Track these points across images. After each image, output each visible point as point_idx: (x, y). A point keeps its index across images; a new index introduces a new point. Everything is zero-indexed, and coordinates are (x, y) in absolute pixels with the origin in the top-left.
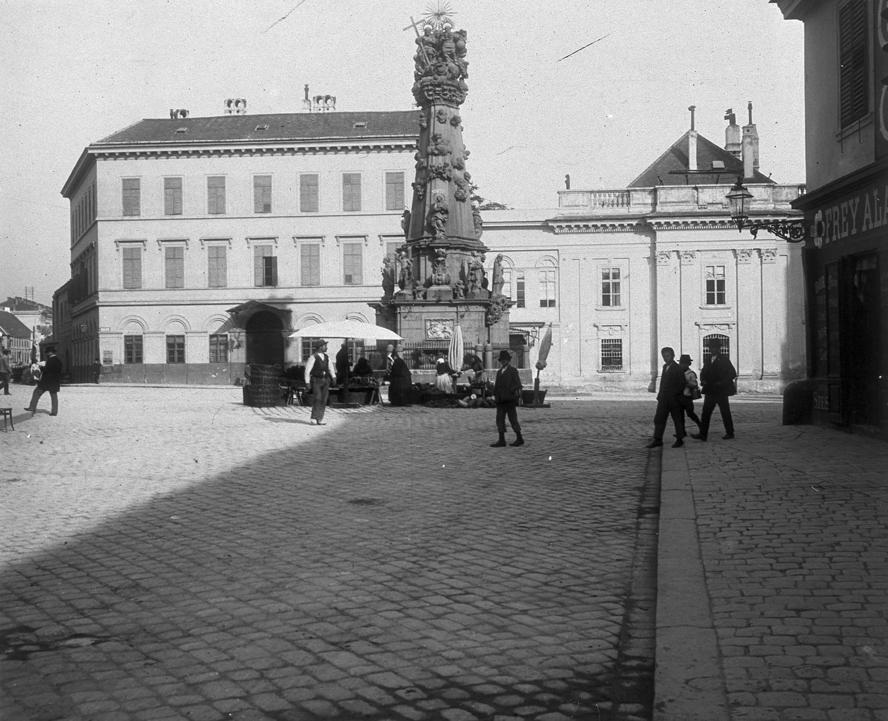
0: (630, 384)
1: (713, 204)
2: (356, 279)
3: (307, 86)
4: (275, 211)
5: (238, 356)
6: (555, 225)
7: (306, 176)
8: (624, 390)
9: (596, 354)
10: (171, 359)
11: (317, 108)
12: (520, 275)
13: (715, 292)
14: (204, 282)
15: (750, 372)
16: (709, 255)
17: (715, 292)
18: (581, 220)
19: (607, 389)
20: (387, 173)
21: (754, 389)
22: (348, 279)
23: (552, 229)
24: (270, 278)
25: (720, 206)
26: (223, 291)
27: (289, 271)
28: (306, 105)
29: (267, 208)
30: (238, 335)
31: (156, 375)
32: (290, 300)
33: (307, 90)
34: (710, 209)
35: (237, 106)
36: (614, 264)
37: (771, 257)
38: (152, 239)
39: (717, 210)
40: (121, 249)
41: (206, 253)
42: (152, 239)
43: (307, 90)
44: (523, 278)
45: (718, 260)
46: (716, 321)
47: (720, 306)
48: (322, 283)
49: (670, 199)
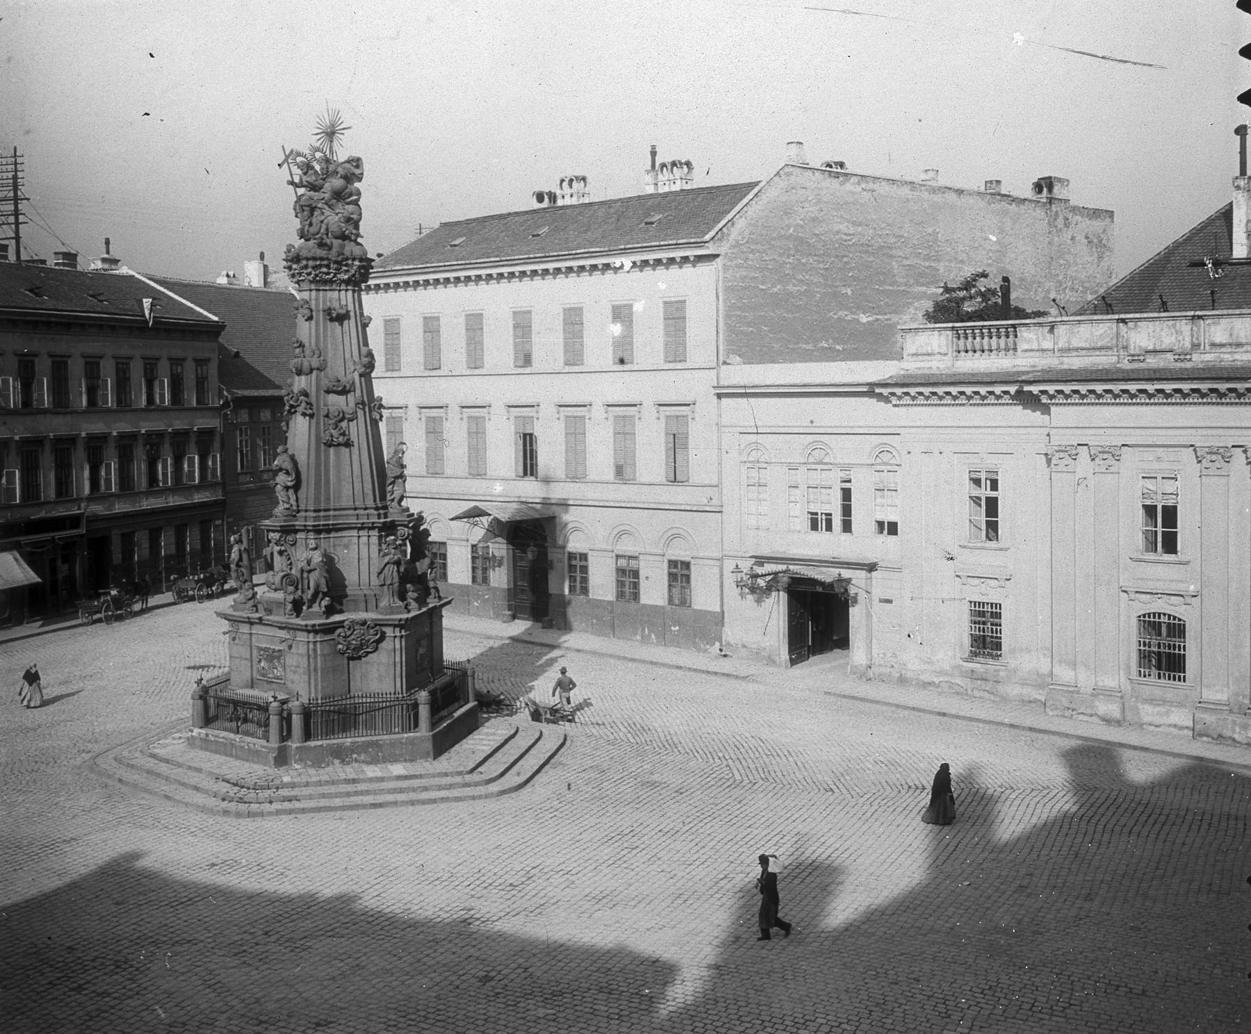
0: (1014, 691)
1: (1155, 351)
2: (628, 471)
3: (653, 147)
4: (537, 365)
5: (500, 578)
6: (885, 391)
7: (570, 309)
8: (1005, 699)
9: (961, 630)
10: (620, 595)
11: (671, 183)
12: (843, 475)
13: (1163, 528)
14: (463, 469)
15: (1223, 697)
16: (1149, 455)
17: (1163, 528)
18: (896, 385)
19: (976, 693)
20: (665, 303)
21: (1227, 733)
22: (619, 470)
23: (880, 397)
24: (529, 466)
25: (1170, 356)
26: (439, 480)
27: (550, 456)
28: (649, 178)
29: (527, 360)
30: (499, 548)
31: (656, 624)
32: (564, 505)
33: (654, 154)
34: (1152, 362)
35: (571, 186)
36: (991, 462)
37: (1069, 461)
38: (648, 403)
39: (1162, 365)
40: (611, 416)
41: (465, 425)
42: (648, 403)
43: (654, 154)
44: (849, 481)
45: (1165, 466)
46: (1160, 587)
47: (1167, 557)
48: (448, 472)
49: (1076, 343)
